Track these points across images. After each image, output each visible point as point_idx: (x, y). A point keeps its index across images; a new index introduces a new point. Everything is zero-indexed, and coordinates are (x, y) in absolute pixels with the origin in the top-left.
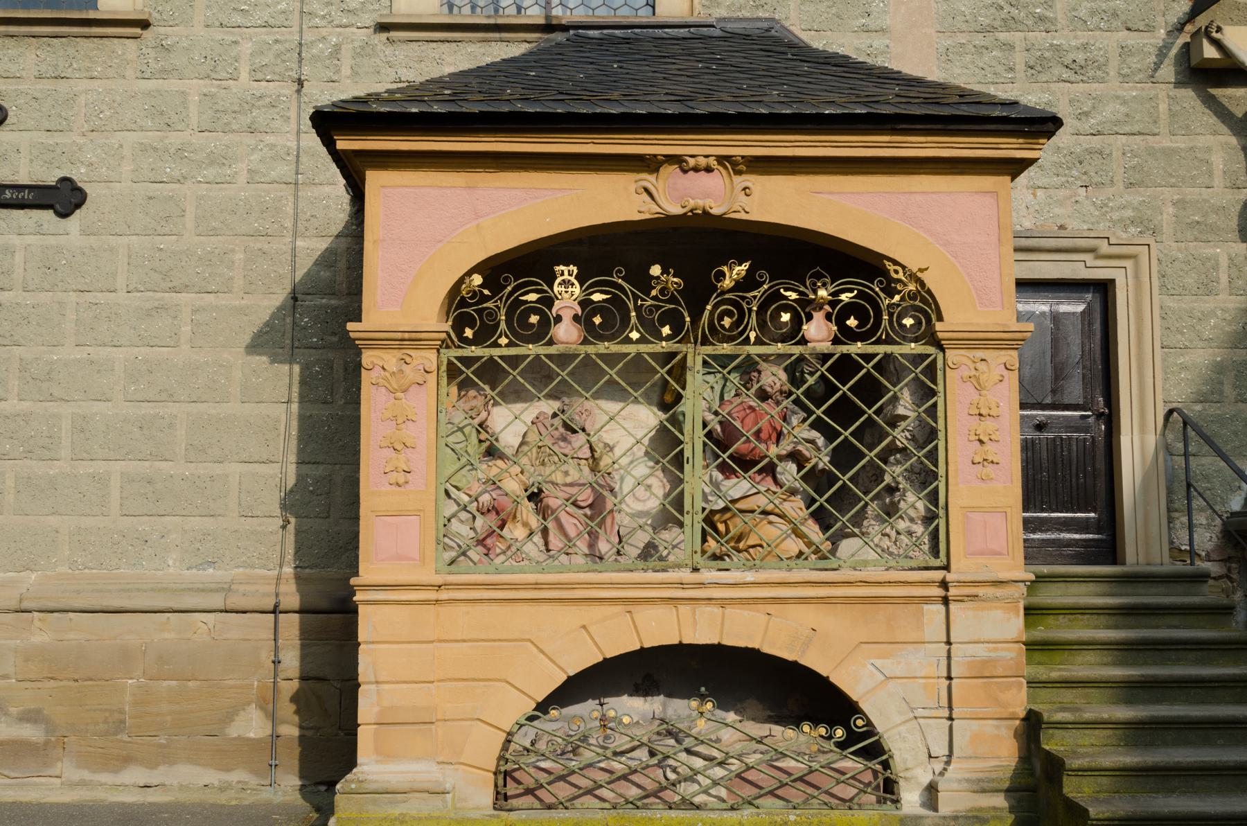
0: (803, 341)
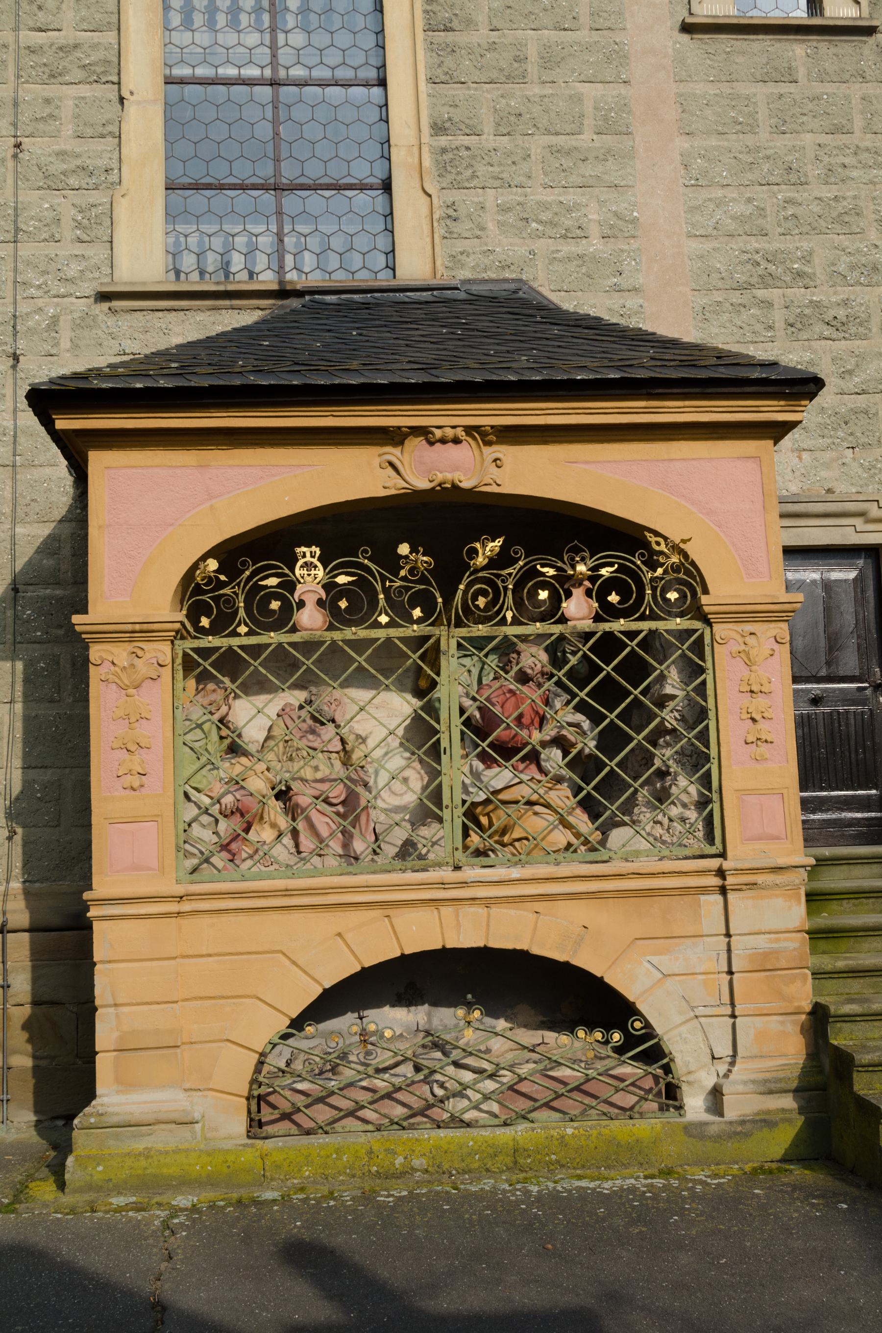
0: (563, 620)
